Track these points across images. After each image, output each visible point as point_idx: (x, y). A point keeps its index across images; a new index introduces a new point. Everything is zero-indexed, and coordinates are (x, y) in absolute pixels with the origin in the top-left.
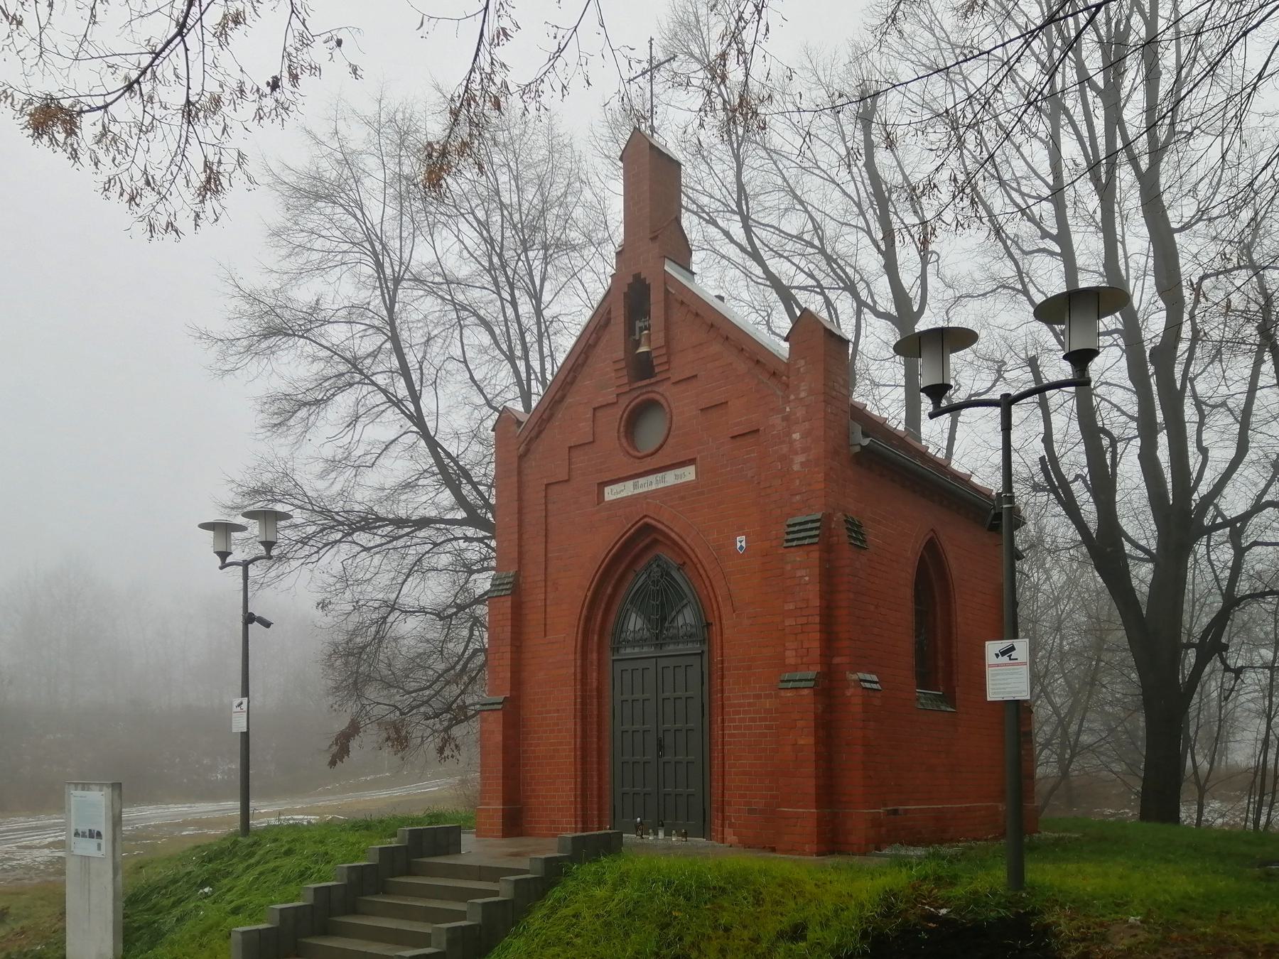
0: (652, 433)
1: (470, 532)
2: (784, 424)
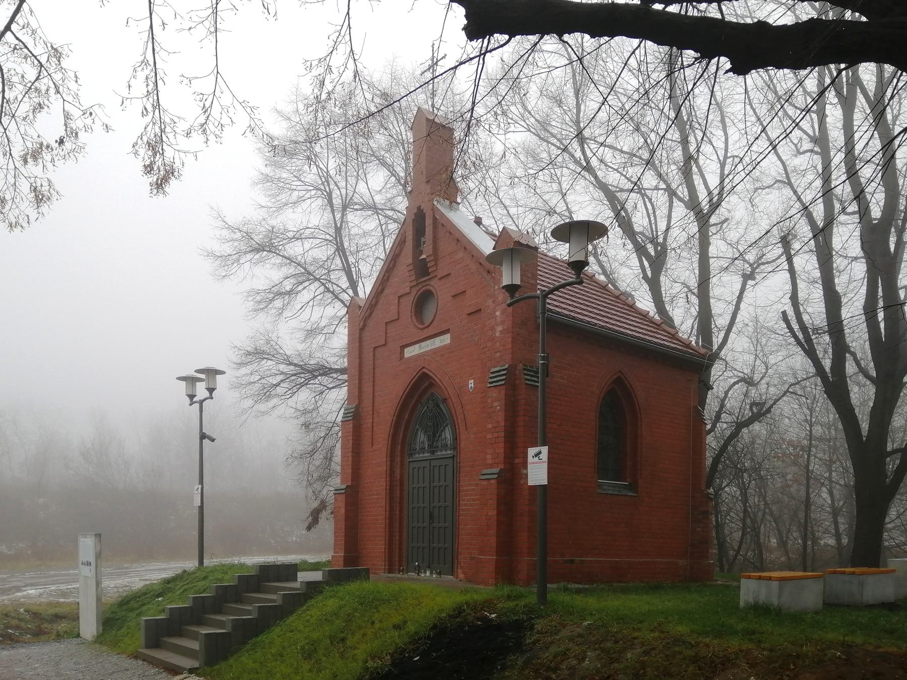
0: (429, 313)
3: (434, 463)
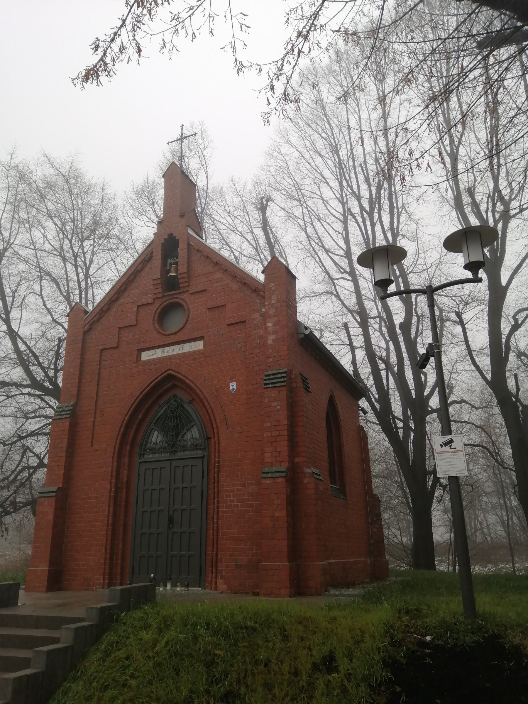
0: (175, 322)
1: (31, 391)
2: (261, 318)
3: (175, 463)
